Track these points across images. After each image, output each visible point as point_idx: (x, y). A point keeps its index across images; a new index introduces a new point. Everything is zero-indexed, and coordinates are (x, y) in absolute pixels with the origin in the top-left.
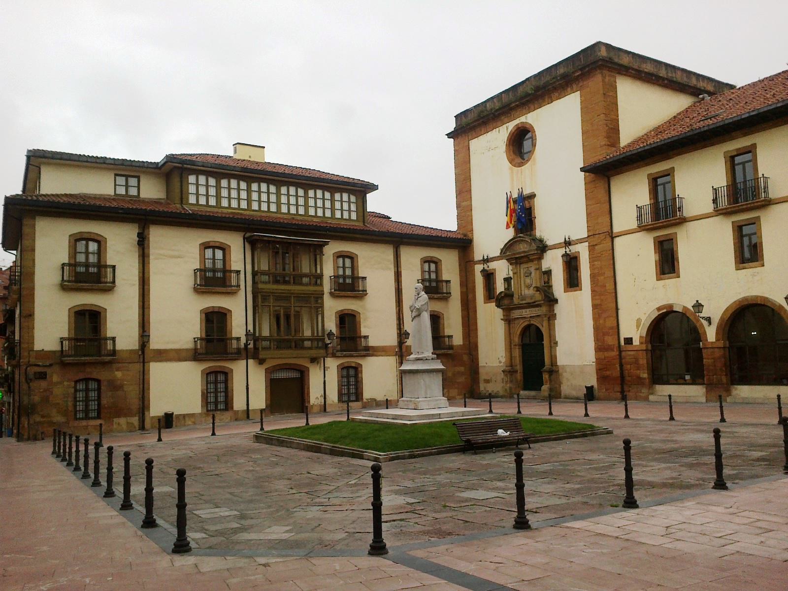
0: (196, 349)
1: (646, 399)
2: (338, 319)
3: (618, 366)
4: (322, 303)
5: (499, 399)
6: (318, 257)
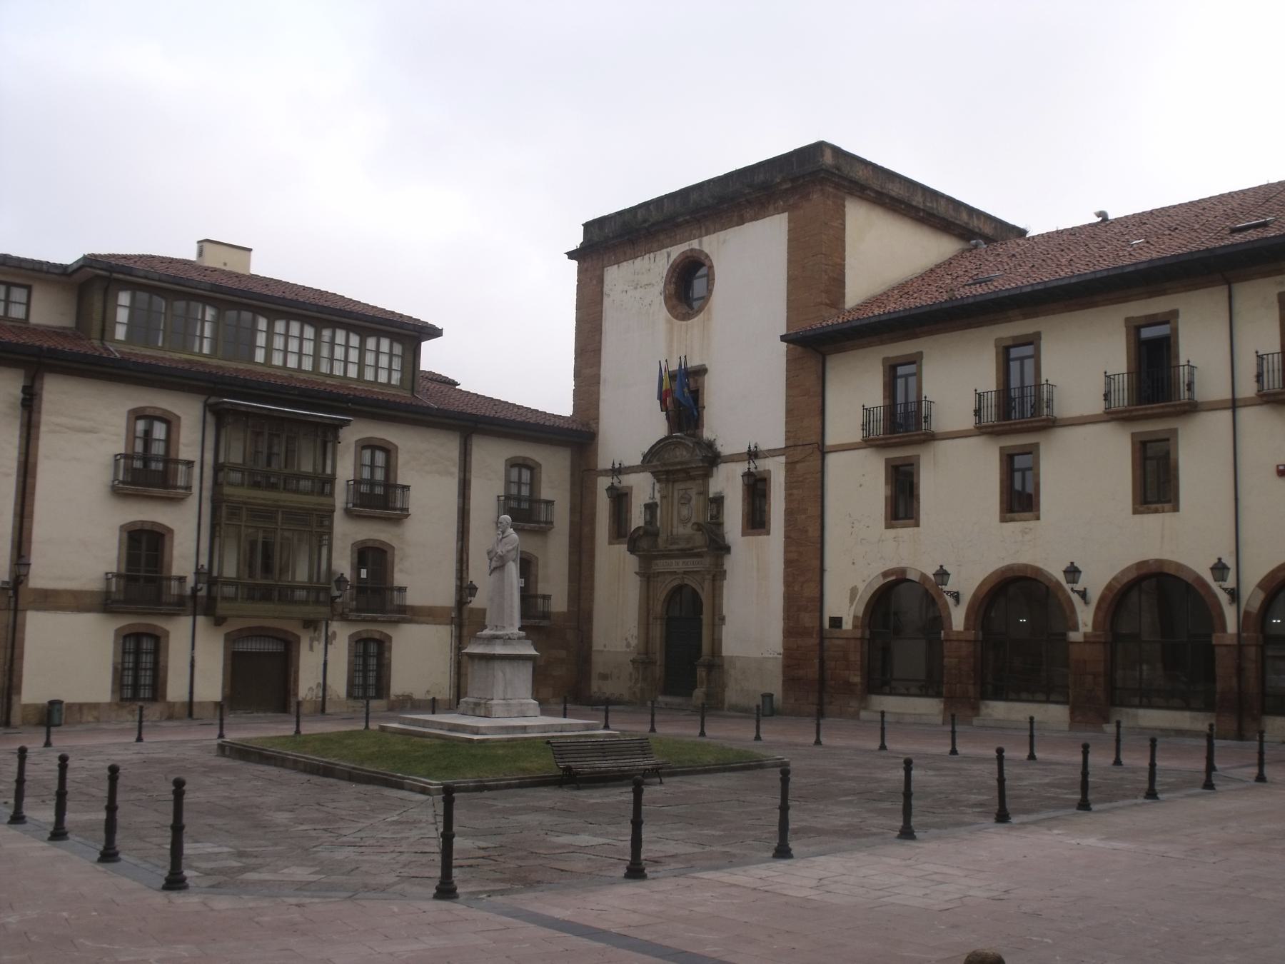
0: (107, 593)
1: (855, 716)
2: (356, 555)
3: (817, 661)
4: (331, 527)
5: (621, 707)
6: (329, 445)
